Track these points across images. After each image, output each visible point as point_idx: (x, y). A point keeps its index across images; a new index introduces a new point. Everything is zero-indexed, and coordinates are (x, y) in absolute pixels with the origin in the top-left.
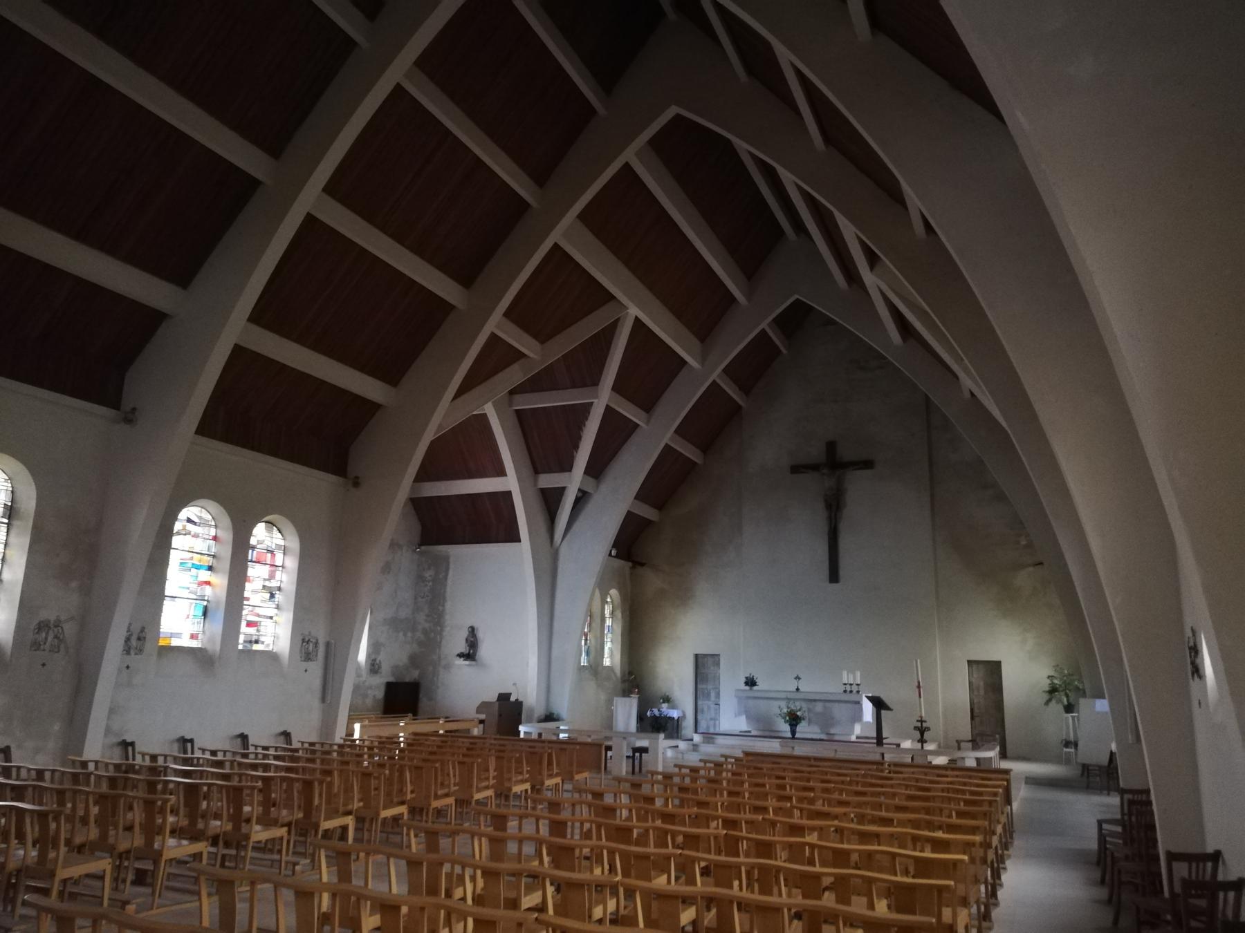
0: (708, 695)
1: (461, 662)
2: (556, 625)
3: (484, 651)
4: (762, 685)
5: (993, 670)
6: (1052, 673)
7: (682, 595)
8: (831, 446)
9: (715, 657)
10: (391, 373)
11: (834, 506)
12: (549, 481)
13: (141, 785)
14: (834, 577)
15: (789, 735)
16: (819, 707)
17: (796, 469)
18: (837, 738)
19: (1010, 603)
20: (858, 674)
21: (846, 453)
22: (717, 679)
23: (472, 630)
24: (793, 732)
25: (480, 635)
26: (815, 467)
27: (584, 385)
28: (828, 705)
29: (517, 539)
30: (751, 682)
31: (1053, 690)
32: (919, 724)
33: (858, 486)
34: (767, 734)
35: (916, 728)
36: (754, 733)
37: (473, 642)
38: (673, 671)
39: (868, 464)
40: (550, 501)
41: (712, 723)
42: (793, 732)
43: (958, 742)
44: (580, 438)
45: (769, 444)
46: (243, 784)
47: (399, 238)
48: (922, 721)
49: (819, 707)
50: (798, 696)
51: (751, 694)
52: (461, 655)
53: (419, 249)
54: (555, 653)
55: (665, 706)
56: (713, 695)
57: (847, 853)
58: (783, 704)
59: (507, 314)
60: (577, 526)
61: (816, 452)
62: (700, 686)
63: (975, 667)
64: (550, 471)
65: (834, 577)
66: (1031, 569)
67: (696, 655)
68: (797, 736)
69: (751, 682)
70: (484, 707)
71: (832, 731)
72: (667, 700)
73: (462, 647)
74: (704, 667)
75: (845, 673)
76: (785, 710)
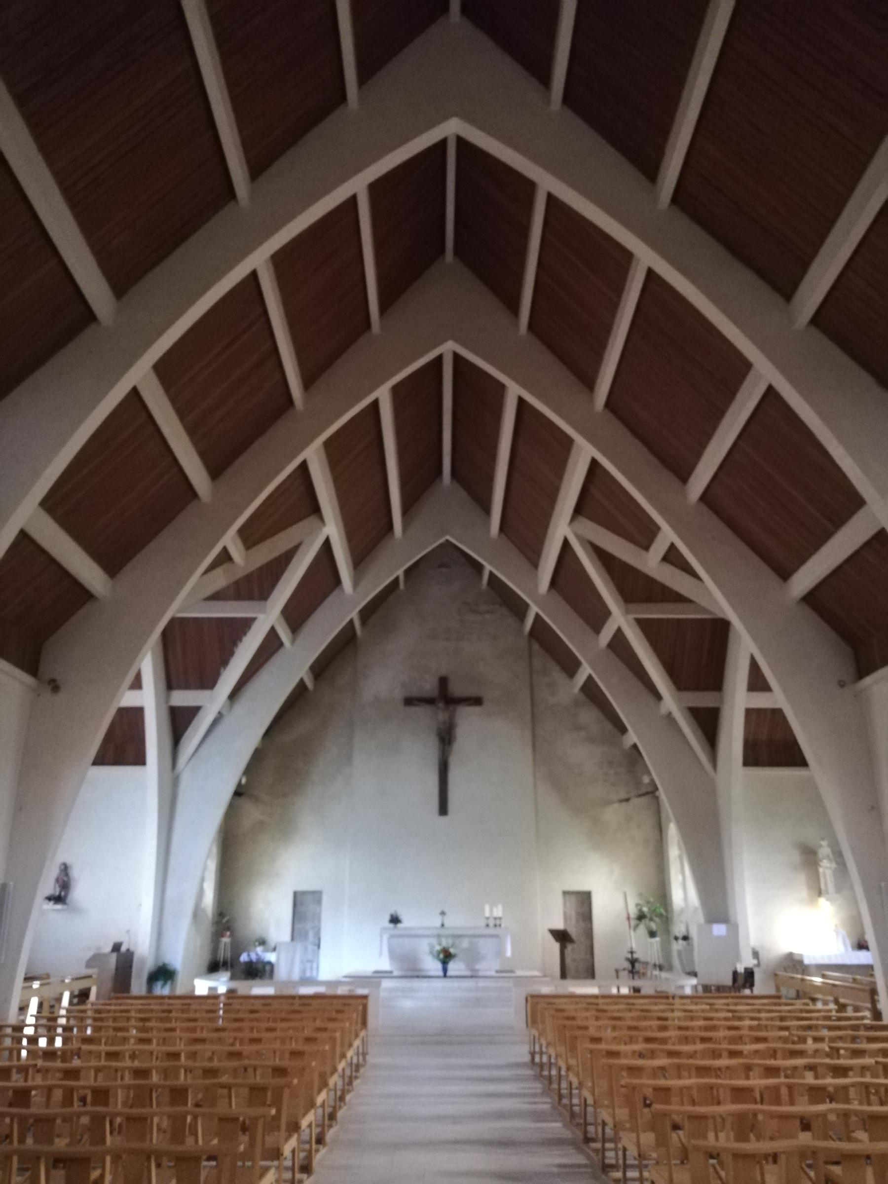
0: (306, 934)
1: (51, 906)
2: (173, 861)
3: (79, 893)
4: (407, 922)
5: (584, 899)
6: (640, 902)
7: (284, 828)
8: (443, 682)
9: (316, 896)
10: (113, 562)
11: (446, 738)
12: (182, 698)
13: (852, 1093)
14: (443, 809)
15: (441, 973)
16: (465, 943)
17: (409, 701)
18: (480, 974)
19: (600, 837)
20: (500, 907)
21: (457, 689)
22: (317, 917)
23: (65, 869)
24: (445, 970)
25: (75, 873)
26: (429, 701)
27: (251, 598)
28: (475, 940)
29: (140, 760)
30: (395, 920)
31: (641, 917)
32: (629, 956)
33: (468, 721)
34: (409, 973)
35: (628, 959)
36: (396, 973)
37: (65, 883)
38: (269, 911)
39: (477, 701)
40: (179, 721)
41: (308, 965)
42: (445, 970)
43: (617, 971)
44: (231, 654)
45: (384, 677)
46: (30, 1083)
47: (182, 414)
48: (632, 953)
49: (465, 943)
50: (443, 932)
51: (396, 932)
52: (49, 899)
53: (192, 431)
54: (170, 892)
55: (259, 949)
56: (311, 935)
57: (749, 1090)
58: (434, 941)
59: (579, 510)
60: (203, 751)
61: (429, 686)
62: (297, 926)
63: (568, 897)
64: (187, 687)
65: (443, 809)
66: (616, 806)
67: (296, 894)
68: (449, 973)
69: (395, 920)
70: (95, 960)
71: (477, 967)
72: (263, 942)
73: (49, 886)
74: (304, 906)
75: (487, 908)
76: (438, 948)
